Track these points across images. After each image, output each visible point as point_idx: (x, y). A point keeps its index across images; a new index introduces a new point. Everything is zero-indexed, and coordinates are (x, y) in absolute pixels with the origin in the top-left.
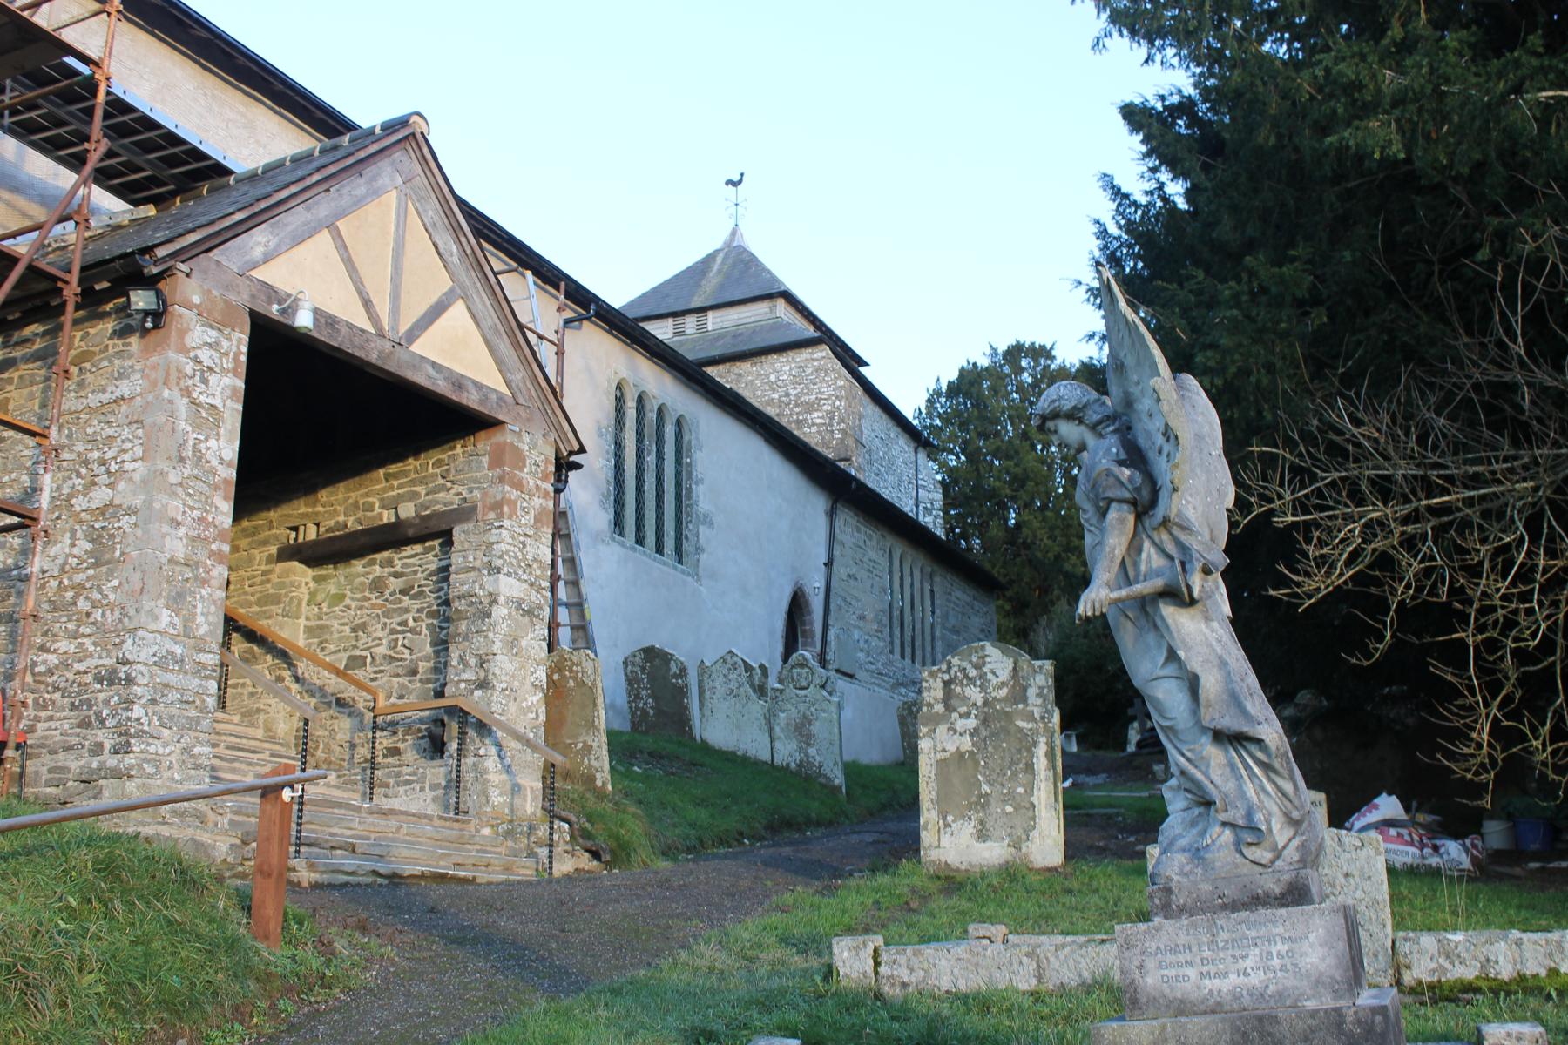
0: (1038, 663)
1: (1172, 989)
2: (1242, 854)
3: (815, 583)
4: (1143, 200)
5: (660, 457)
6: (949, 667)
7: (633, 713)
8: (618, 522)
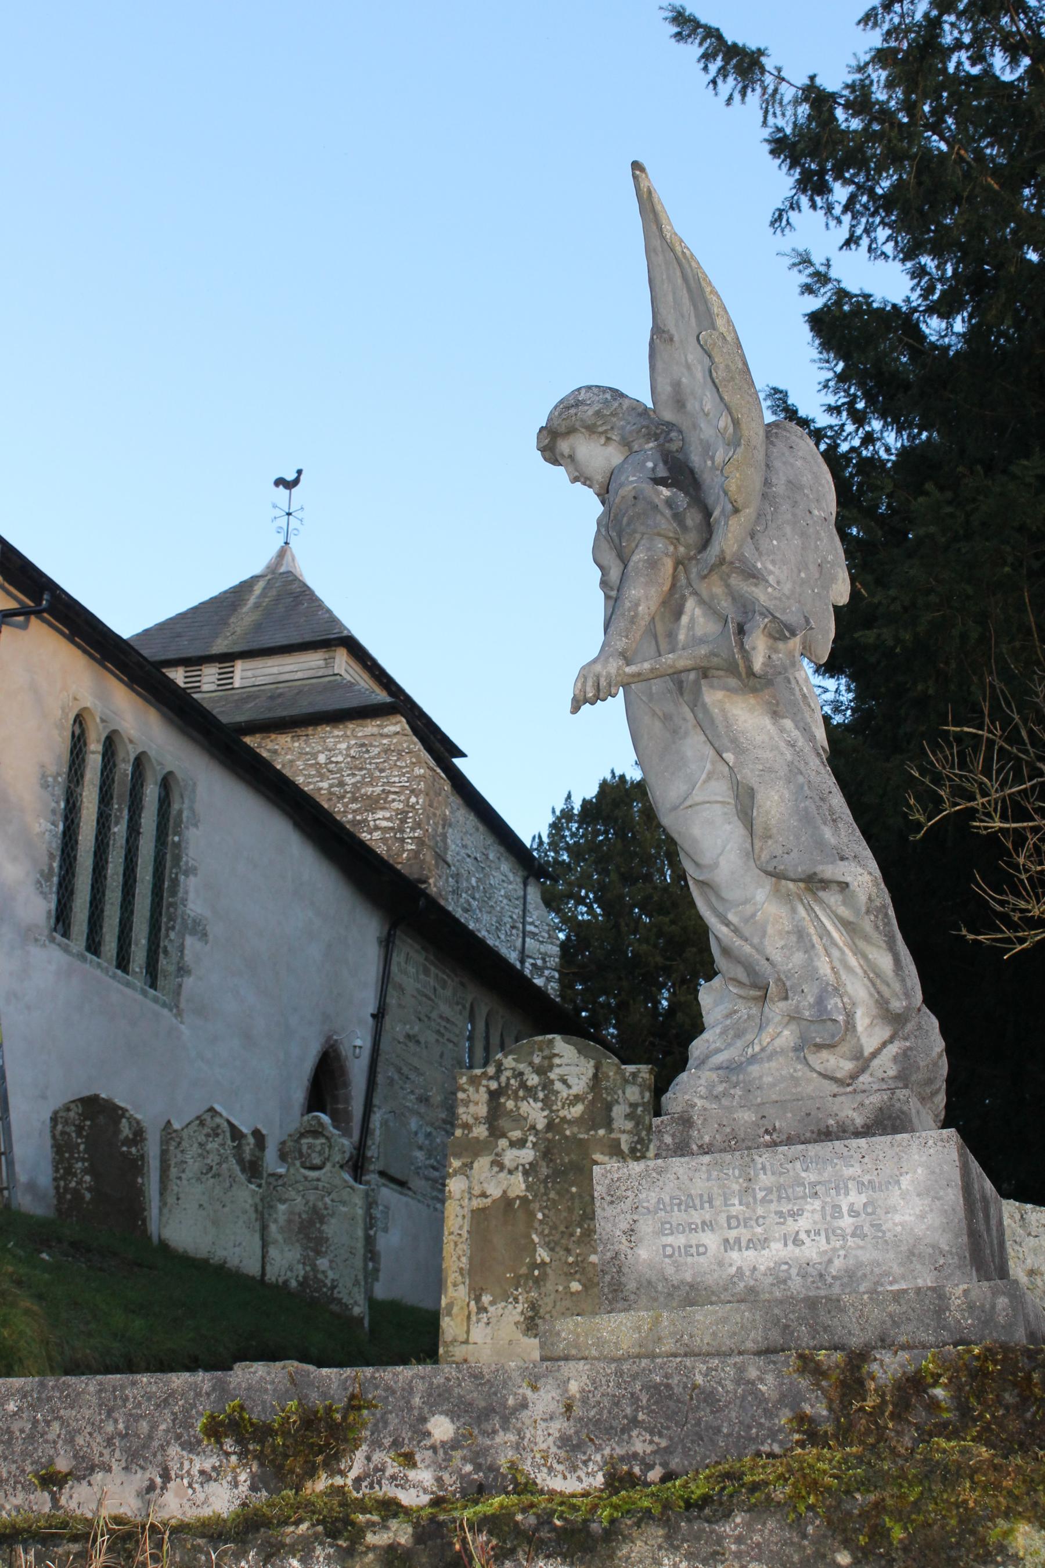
0: (631, 1068)
1: (678, 1267)
2: (808, 1064)
3: (358, 1040)
4: (823, 420)
5: (134, 830)
6: (499, 1070)
7: (60, 1196)
8: (62, 918)
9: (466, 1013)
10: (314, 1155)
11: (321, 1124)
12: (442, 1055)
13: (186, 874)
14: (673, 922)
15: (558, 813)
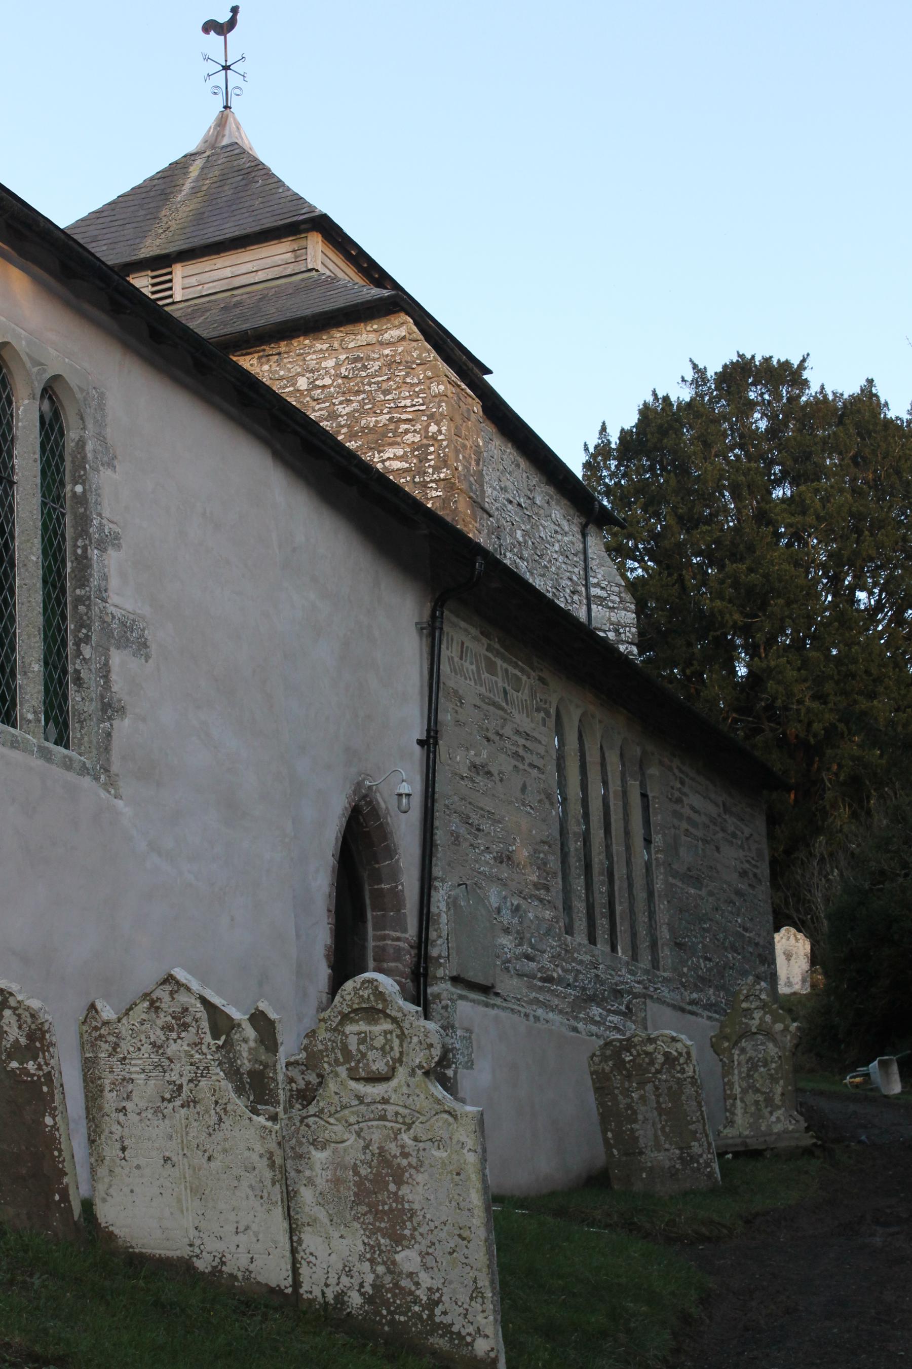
3: (402, 782)
9: (551, 722)
10: (371, 1055)
11: (380, 995)
12: (524, 788)
13: (102, 546)
14: (751, 570)
15: (592, 450)
